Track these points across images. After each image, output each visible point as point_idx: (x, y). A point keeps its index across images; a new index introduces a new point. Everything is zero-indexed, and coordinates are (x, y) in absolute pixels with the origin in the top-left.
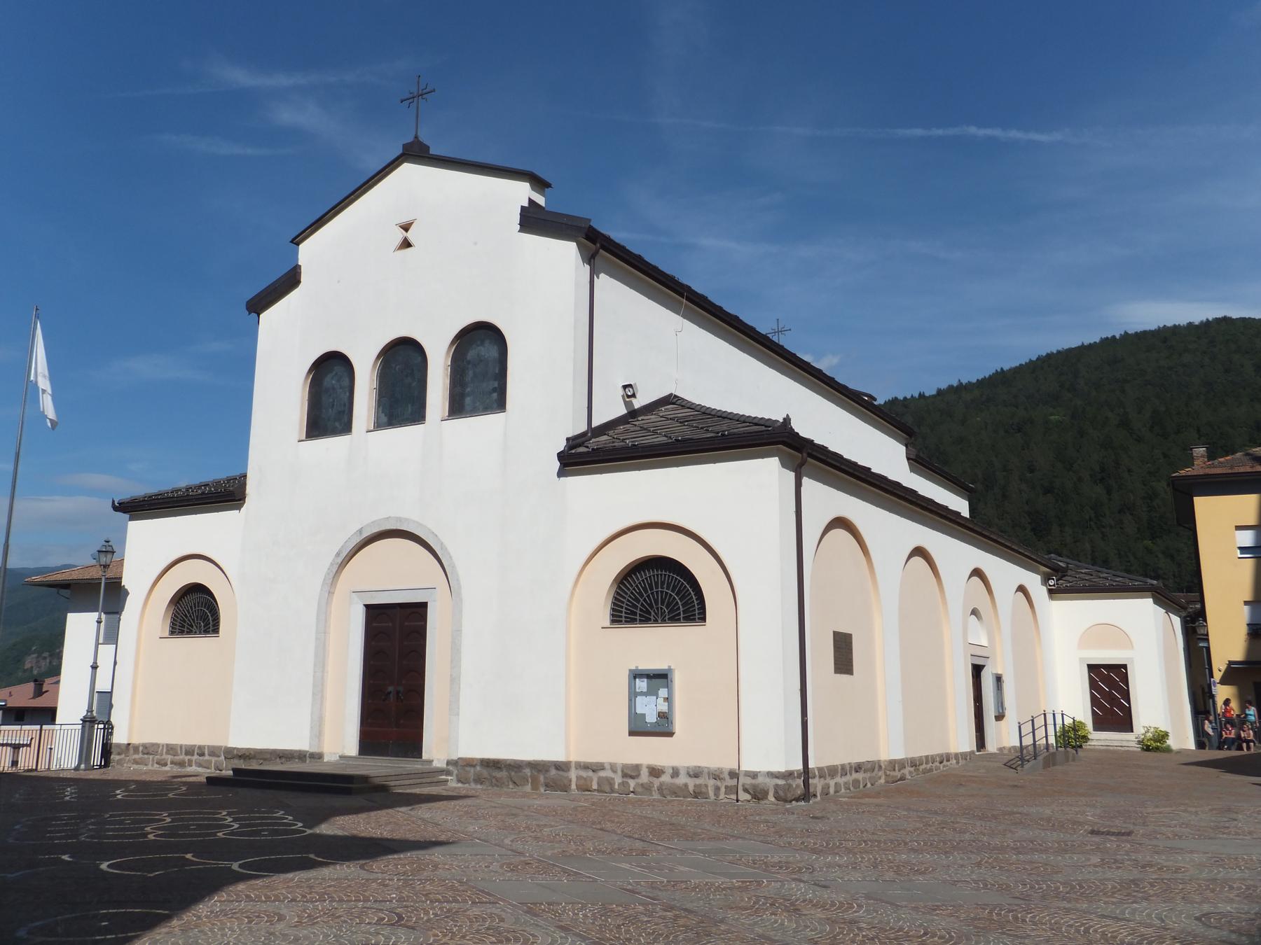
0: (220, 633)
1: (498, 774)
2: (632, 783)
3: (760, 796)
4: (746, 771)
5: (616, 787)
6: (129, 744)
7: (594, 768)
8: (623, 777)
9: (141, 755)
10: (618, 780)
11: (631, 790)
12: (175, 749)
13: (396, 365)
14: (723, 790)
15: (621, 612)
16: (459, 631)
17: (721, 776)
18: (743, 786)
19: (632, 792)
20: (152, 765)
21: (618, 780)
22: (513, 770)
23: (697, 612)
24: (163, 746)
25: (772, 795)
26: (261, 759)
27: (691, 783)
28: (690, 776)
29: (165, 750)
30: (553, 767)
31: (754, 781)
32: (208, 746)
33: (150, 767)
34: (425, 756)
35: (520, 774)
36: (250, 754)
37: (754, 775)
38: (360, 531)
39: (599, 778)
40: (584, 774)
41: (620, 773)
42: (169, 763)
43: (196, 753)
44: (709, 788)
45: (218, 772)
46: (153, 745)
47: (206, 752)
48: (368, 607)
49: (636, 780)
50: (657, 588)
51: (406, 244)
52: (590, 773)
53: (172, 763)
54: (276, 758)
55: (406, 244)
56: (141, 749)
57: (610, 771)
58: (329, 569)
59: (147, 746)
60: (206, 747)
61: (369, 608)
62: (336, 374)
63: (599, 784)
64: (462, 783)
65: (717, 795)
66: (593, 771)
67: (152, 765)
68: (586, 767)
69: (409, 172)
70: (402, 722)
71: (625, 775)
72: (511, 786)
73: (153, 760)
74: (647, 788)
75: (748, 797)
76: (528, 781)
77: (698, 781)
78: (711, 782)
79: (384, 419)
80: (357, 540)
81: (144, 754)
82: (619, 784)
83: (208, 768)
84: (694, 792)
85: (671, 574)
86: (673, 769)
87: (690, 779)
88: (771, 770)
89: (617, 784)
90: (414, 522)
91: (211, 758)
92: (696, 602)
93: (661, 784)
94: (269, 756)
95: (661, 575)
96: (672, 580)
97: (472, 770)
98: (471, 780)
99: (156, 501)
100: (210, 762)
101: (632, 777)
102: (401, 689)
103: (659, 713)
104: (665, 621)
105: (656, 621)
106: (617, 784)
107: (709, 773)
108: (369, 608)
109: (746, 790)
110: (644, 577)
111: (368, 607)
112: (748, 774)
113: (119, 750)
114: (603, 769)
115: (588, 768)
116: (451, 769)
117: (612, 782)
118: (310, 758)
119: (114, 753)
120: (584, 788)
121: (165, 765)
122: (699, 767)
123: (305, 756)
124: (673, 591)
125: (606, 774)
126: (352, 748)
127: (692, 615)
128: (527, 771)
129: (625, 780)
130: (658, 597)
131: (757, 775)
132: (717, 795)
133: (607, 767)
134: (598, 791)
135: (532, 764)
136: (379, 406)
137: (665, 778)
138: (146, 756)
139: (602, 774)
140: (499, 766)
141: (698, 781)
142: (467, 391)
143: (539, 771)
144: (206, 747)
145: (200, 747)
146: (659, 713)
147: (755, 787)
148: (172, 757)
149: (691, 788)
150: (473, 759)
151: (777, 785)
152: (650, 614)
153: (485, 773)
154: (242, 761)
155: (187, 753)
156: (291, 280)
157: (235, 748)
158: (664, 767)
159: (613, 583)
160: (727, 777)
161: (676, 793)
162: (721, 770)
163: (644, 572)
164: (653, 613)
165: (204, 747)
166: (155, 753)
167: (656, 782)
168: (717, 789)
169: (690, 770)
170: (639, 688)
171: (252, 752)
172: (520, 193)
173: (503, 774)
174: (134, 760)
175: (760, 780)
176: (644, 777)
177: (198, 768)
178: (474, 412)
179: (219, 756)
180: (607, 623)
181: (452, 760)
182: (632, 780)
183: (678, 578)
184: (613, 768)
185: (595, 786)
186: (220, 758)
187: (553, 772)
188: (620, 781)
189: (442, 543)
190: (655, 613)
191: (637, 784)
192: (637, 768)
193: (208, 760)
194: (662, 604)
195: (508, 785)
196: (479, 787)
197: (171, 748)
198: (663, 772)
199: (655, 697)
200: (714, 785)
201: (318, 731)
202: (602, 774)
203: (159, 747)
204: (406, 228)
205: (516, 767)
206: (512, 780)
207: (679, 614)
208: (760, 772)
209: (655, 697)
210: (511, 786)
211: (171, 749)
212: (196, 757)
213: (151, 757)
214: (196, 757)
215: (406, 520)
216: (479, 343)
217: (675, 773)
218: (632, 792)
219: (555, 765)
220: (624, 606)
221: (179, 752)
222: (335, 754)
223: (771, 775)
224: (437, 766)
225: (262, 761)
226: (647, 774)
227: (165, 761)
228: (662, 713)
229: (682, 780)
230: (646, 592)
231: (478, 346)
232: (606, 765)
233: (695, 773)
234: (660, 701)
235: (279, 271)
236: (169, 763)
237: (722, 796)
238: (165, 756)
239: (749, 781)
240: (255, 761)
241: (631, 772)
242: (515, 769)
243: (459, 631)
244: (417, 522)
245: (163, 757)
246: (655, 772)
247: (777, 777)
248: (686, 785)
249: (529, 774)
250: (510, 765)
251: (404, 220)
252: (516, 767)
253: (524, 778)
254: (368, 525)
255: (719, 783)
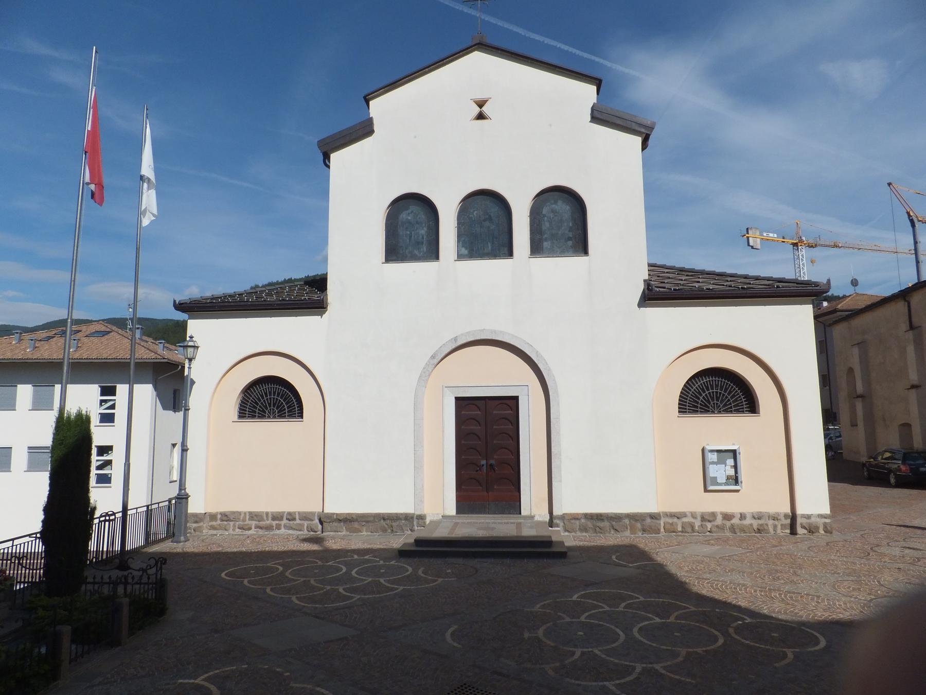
0: (761, 413)
1: (601, 524)
2: (709, 525)
3: (814, 531)
4: (802, 514)
5: (697, 528)
6: (205, 513)
7: (679, 516)
8: (702, 521)
9: (219, 522)
10: (697, 523)
11: (709, 530)
12: (261, 516)
13: (474, 211)
14: (779, 527)
15: (246, 411)
16: (557, 418)
17: (779, 518)
18: (801, 524)
19: (709, 531)
20: (234, 530)
21: (697, 523)
22: (613, 521)
23: (297, 412)
24: (245, 513)
25: (822, 529)
26: (363, 522)
27: (755, 524)
28: (755, 518)
29: (248, 517)
30: (648, 517)
31: (808, 521)
32: (298, 512)
33: (231, 532)
34: (524, 512)
35: (621, 523)
36: (352, 518)
37: (808, 517)
38: (455, 339)
39: (683, 523)
40: (670, 520)
41: (699, 518)
42: (253, 527)
43: (285, 518)
44: (769, 526)
45: (312, 533)
46: (234, 513)
47: (297, 517)
48: (457, 399)
49: (713, 523)
50: (270, 395)
51: (481, 116)
52: (675, 520)
53: (257, 527)
54: (380, 520)
55: (481, 116)
56: (219, 516)
57: (691, 518)
58: (424, 368)
59: (227, 514)
60: (297, 513)
61: (458, 400)
62: (412, 212)
63: (682, 527)
64: (569, 532)
65: (775, 530)
66: (678, 518)
67: (234, 530)
68: (672, 515)
69: (477, 58)
70: (463, 487)
71: (703, 519)
72: (612, 533)
73: (234, 526)
74: (720, 528)
75: (805, 531)
76: (627, 528)
77: (760, 522)
78: (771, 522)
79: (464, 251)
80: (454, 346)
81: (222, 520)
82: (699, 526)
83: (300, 530)
84: (758, 529)
85: (280, 387)
86: (741, 514)
87: (755, 520)
88: (820, 513)
89: (697, 526)
90: (509, 334)
91: (303, 522)
92: (295, 403)
93: (732, 525)
94: (372, 519)
95: (715, 380)
96: (276, 390)
97: (577, 522)
98: (577, 529)
99: (257, 303)
100: (302, 525)
101: (709, 521)
102: (492, 462)
103: (727, 476)
104: (276, 417)
105: (269, 417)
106: (697, 526)
107: (769, 517)
108: (458, 400)
109: (803, 527)
110: (264, 387)
111: (457, 399)
112: (803, 516)
113: (196, 519)
114: (685, 517)
115: (675, 516)
116: (558, 522)
117: (692, 524)
118: (417, 518)
119: (190, 522)
120: (670, 529)
121: (250, 529)
122: (761, 512)
123: (412, 518)
124: (281, 398)
125: (688, 519)
126: (451, 508)
127: (283, 414)
128: (627, 521)
129: (703, 523)
130: (266, 404)
131: (810, 517)
132: (775, 530)
133: (689, 515)
134: (682, 532)
135: (630, 516)
136: (458, 241)
137: (735, 521)
138: (225, 523)
139: (685, 520)
140: (603, 518)
141: (760, 522)
142: (544, 237)
143: (636, 521)
144: (297, 513)
145: (289, 514)
146: (727, 476)
147: (810, 524)
148: (257, 522)
149: (755, 527)
150: (578, 514)
151: (825, 523)
152: (265, 413)
153: (590, 524)
154: (342, 523)
155: (274, 518)
156: (365, 129)
157: (334, 514)
158: (733, 513)
159: (240, 394)
160: (783, 518)
161: (744, 531)
162: (778, 514)
163: (259, 385)
164: (267, 412)
165: (295, 513)
166: (235, 520)
167: (728, 524)
168: (775, 527)
169: (755, 515)
170: (711, 460)
171: (354, 517)
172: (587, 93)
173: (606, 524)
174: (211, 525)
175: (813, 520)
176: (719, 520)
177: (287, 531)
178: (552, 253)
179: (312, 520)
180: (236, 418)
181: (558, 515)
182: (709, 523)
183: (285, 390)
184: (693, 515)
185: (680, 529)
186: (314, 522)
187: (649, 520)
188: (699, 524)
189: (537, 352)
190: (269, 412)
191: (713, 525)
192: (713, 514)
193: (300, 524)
194: (274, 406)
195: (610, 531)
196: (584, 534)
197: (256, 515)
198: (734, 517)
199: (724, 465)
200: (773, 524)
201: (418, 497)
202: (685, 520)
203: (240, 514)
204: (481, 104)
205: (616, 519)
206: (613, 528)
207: (285, 413)
208: (812, 515)
209: (724, 465)
210: (612, 533)
211: (254, 516)
212: (285, 521)
213: (232, 523)
214: (285, 521)
215: (501, 332)
216: (553, 202)
217: (743, 517)
218: (709, 531)
219: (650, 515)
220: (688, 401)
221: (265, 518)
222: (438, 514)
223: (821, 516)
224: (539, 520)
225: (364, 523)
226: (721, 518)
227: (249, 526)
228: (730, 476)
229: (748, 521)
230: (263, 398)
231: (552, 204)
232: (697, 513)
233: (758, 516)
234: (728, 468)
235: (349, 122)
236: (253, 527)
237: (779, 531)
238: (247, 522)
239: (804, 521)
240: (357, 523)
241: (707, 518)
242: (616, 520)
243: (557, 418)
244: (512, 335)
245: (246, 523)
246: (727, 517)
247: (826, 518)
248: (751, 525)
249: (628, 523)
250: (611, 517)
251: (480, 96)
252: (616, 519)
253: (625, 526)
254: (462, 334)
255: (776, 522)
